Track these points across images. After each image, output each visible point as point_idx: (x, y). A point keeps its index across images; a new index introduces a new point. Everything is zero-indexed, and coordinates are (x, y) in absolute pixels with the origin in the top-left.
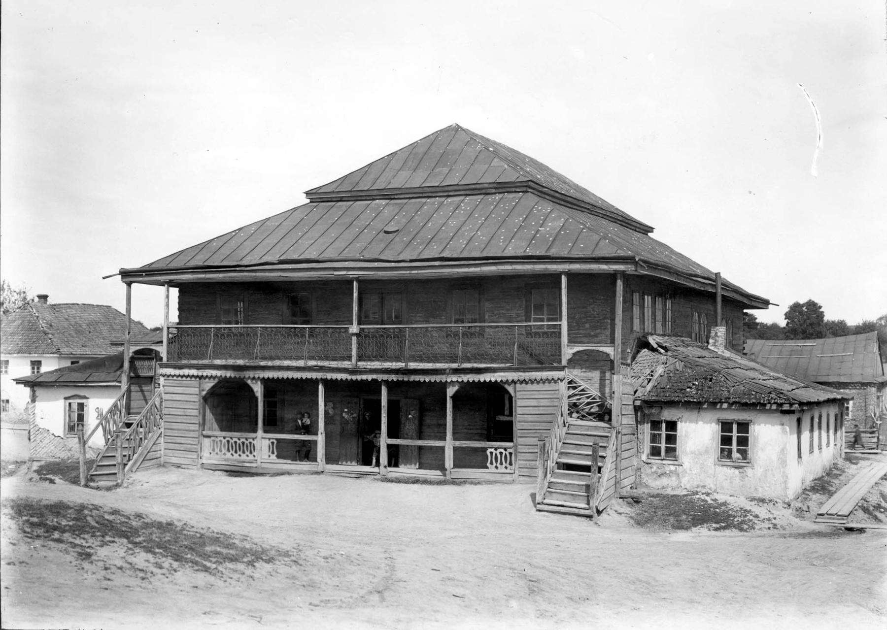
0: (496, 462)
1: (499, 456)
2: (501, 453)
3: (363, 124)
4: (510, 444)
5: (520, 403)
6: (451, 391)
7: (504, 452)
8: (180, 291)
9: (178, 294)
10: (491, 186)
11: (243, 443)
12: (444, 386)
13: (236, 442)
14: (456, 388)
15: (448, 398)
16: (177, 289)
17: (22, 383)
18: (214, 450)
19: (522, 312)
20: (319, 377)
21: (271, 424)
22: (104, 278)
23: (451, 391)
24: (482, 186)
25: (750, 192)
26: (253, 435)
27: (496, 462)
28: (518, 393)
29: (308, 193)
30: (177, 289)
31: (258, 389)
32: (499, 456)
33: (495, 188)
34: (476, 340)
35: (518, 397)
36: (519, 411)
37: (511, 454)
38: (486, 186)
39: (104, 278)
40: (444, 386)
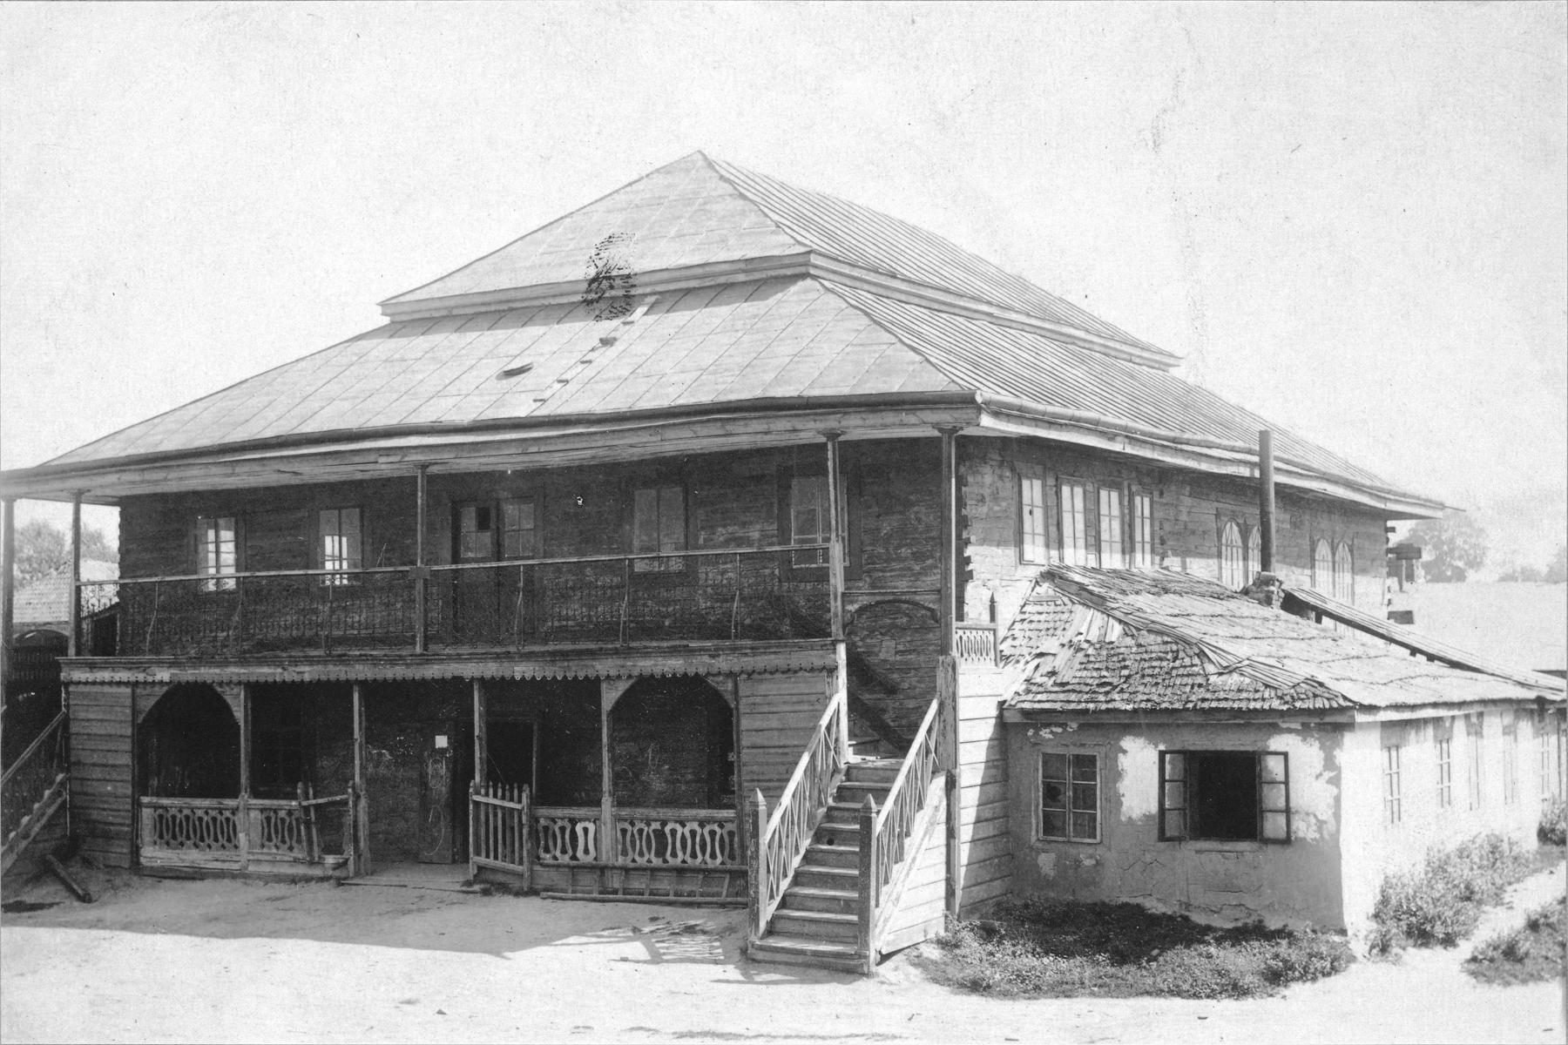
2: (713, 833)
3: (511, 210)
4: (730, 813)
5: (745, 723)
6: (610, 697)
7: (629, 828)
8: (121, 514)
9: (118, 519)
12: (592, 687)
14: (623, 686)
15: (604, 718)
16: (116, 510)
20: (352, 676)
23: (610, 697)
25: (440, 1012)
28: (743, 701)
29: (383, 304)
30: (116, 510)
33: (744, 271)
35: (742, 709)
37: (731, 834)
40: (592, 687)
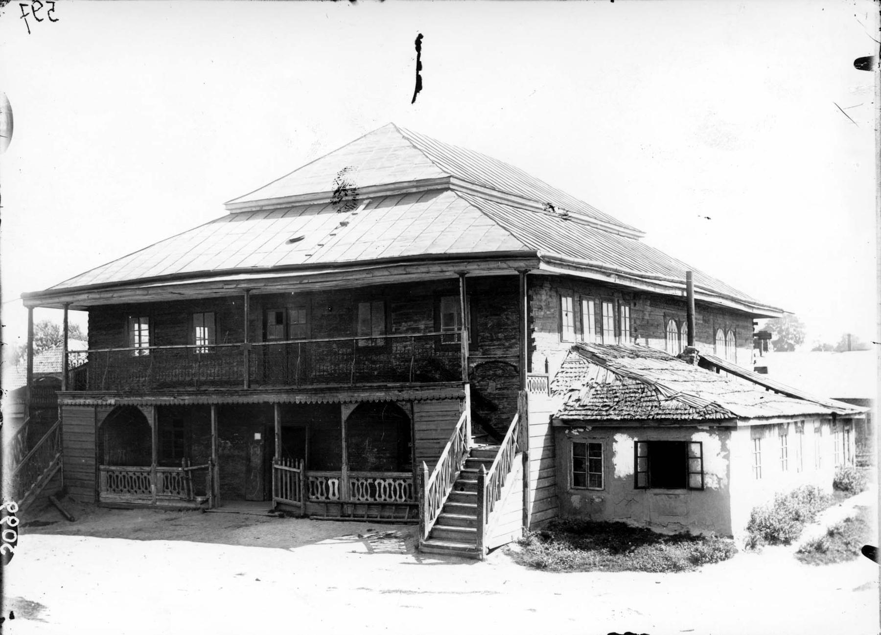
0: (395, 496)
1: (398, 488)
2: (400, 485)
4: (409, 474)
5: (417, 427)
6: (345, 413)
8: (89, 315)
9: (87, 318)
10: (411, 184)
11: (138, 477)
13: (124, 476)
15: (343, 424)
17: (634, 530)
18: (111, 486)
19: (431, 323)
21: (168, 457)
22: (759, 476)
23: (345, 413)
24: (401, 185)
26: (147, 469)
27: (395, 496)
28: (416, 415)
31: (151, 417)
32: (398, 488)
34: (382, 357)
35: (416, 419)
36: (417, 436)
38: (406, 184)
39: (759, 476)
